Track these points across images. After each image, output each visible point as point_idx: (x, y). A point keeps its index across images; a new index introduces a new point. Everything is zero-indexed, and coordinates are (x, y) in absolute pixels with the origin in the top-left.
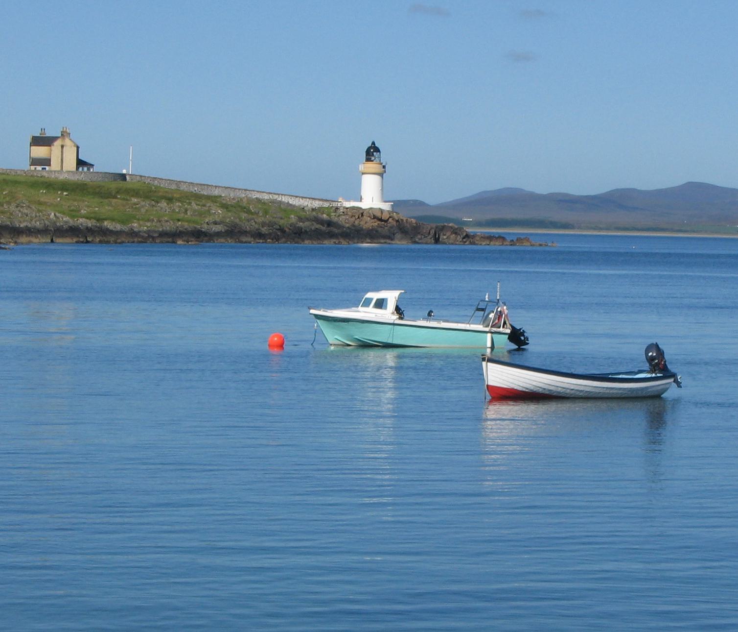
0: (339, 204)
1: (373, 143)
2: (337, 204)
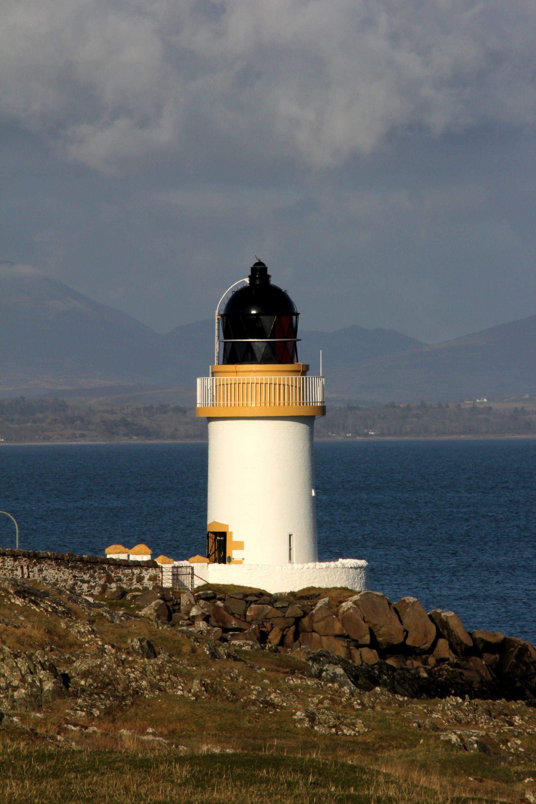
0: (147, 574)
1: (259, 272)
2: (140, 579)
